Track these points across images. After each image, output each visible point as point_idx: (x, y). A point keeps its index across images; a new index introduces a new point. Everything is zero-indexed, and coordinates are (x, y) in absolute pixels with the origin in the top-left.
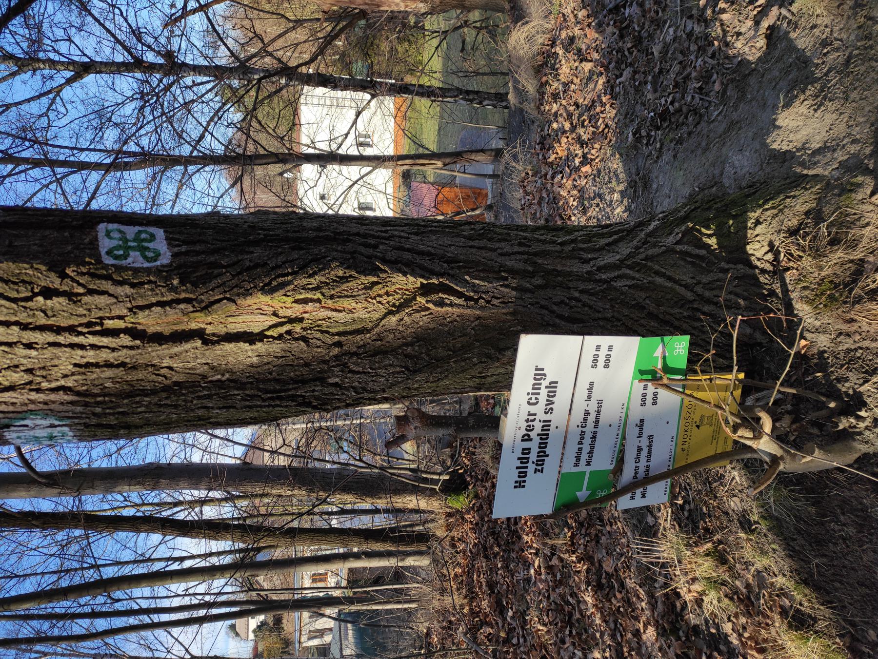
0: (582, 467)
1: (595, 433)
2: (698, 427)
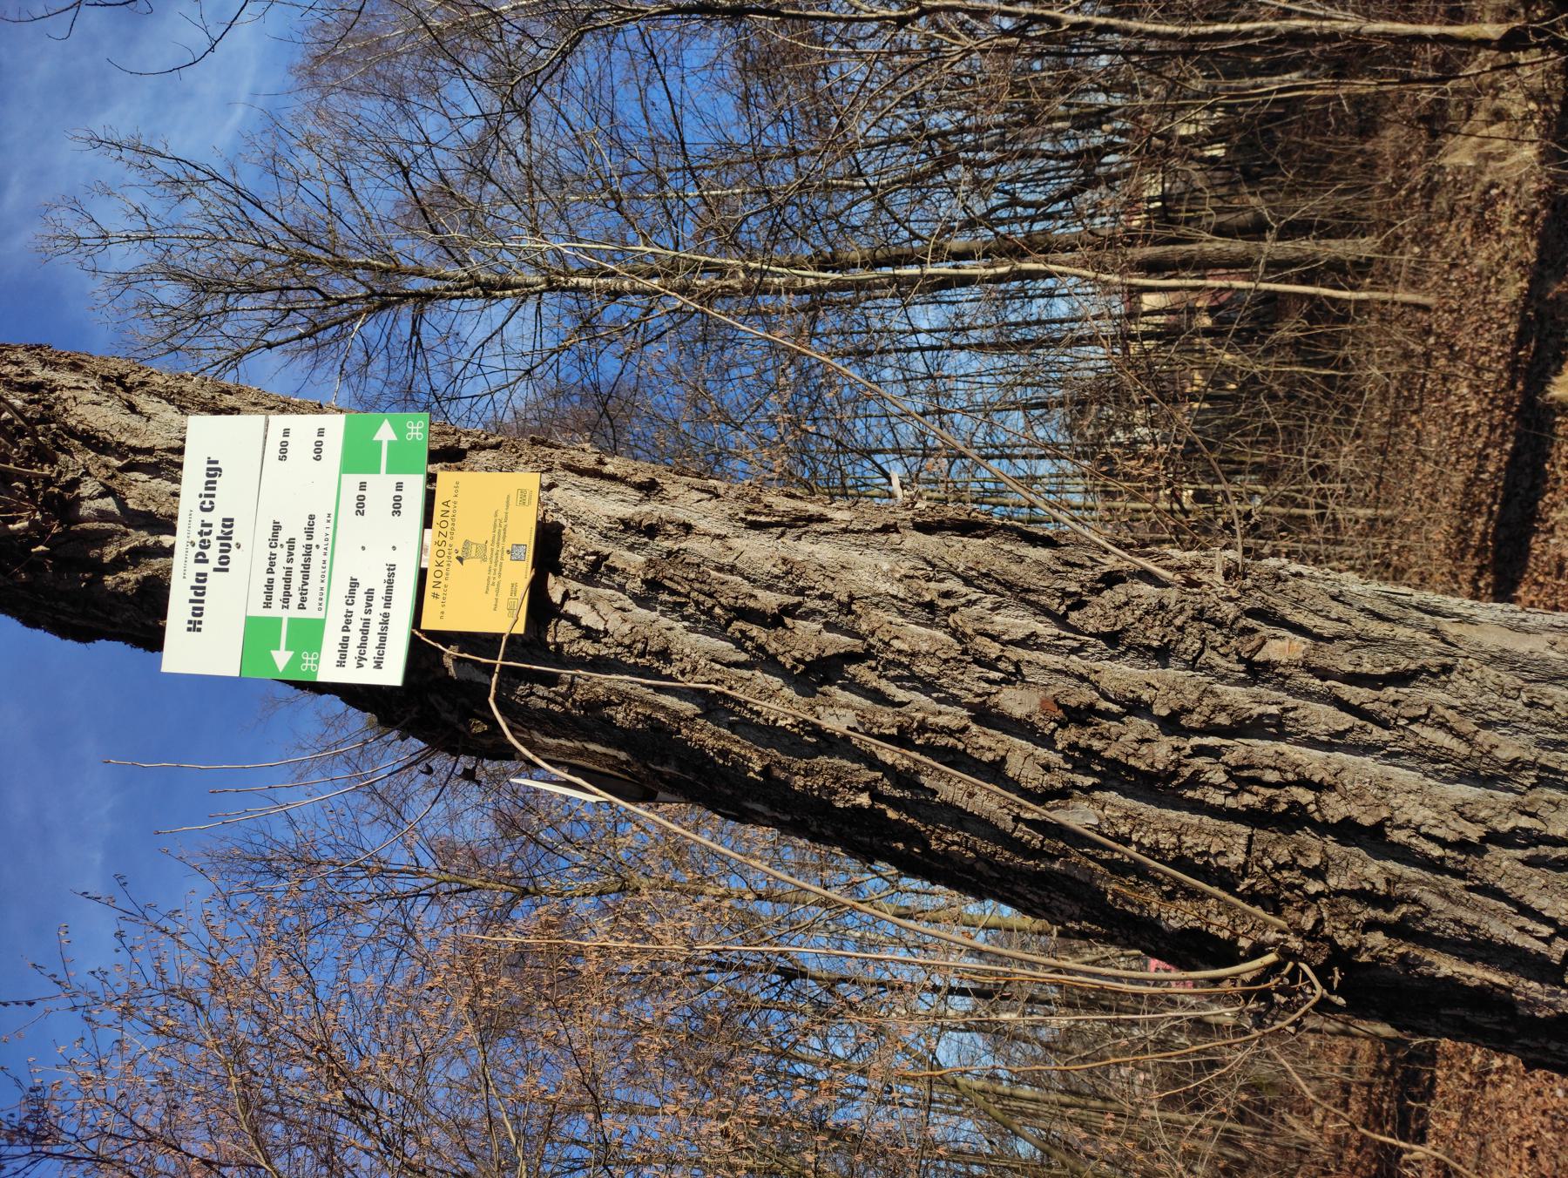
0: (276, 610)
1: (386, 615)
2: (460, 559)
